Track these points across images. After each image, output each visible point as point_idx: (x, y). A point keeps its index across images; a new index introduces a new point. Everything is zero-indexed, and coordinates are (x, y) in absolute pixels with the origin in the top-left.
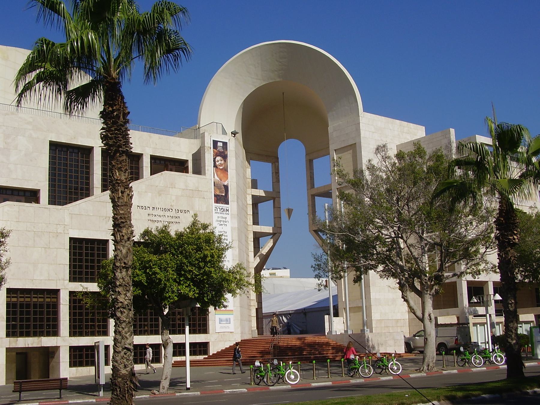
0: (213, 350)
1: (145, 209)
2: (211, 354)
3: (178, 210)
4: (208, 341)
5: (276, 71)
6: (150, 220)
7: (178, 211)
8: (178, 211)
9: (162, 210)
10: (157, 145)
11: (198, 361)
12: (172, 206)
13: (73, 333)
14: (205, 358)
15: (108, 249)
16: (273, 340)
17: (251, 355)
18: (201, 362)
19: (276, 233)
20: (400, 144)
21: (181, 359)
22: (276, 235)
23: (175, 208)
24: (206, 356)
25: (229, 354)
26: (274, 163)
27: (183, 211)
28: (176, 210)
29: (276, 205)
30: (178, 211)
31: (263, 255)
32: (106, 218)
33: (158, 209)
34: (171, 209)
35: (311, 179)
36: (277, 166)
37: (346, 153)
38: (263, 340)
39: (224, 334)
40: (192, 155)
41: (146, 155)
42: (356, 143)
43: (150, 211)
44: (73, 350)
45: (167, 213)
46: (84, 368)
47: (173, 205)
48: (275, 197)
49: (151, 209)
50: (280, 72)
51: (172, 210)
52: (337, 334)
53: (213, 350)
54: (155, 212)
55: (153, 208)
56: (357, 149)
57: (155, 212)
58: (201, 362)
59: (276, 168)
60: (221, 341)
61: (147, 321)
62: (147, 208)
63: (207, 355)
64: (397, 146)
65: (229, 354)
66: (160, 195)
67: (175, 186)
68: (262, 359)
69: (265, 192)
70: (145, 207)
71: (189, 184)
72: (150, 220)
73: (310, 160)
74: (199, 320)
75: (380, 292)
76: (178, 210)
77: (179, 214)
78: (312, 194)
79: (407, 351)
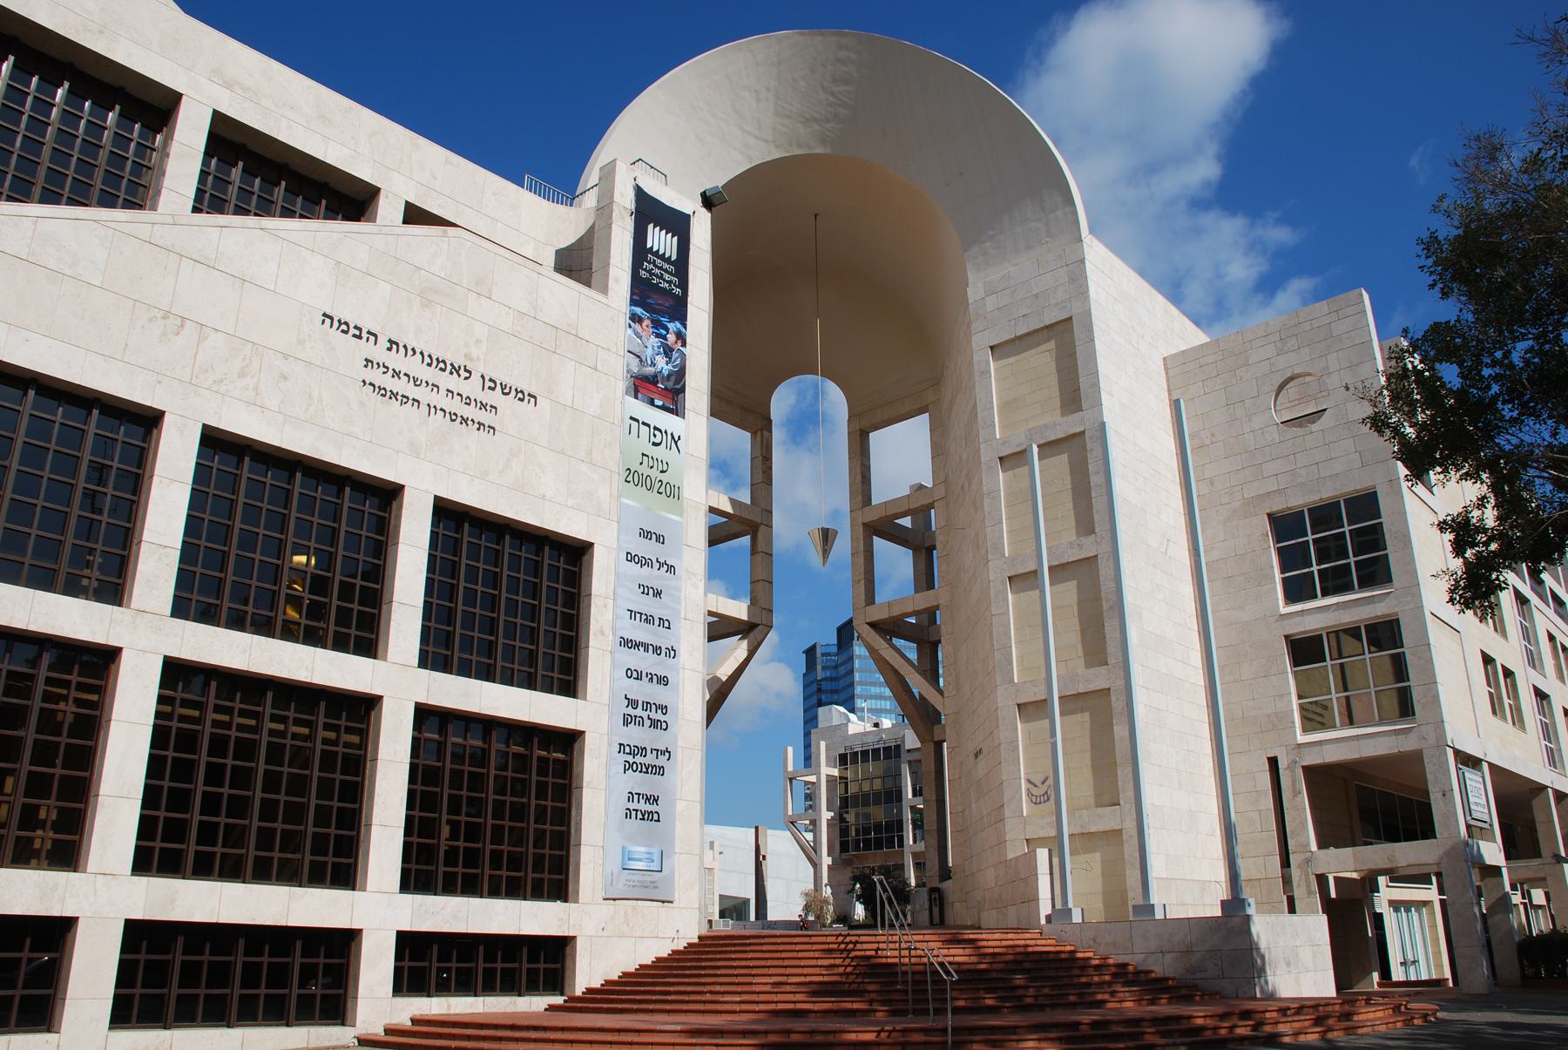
0: (588, 973)
1: (354, 336)
2: (579, 992)
4: (571, 934)
5: (815, 120)
6: (371, 384)
7: (492, 385)
8: (492, 385)
9: (427, 360)
10: (435, 178)
11: (513, 1027)
14: (551, 1008)
17: (780, 1006)
19: (758, 625)
21: (449, 1006)
23: (482, 371)
24: (558, 1000)
25: (669, 993)
27: (513, 392)
28: (483, 377)
29: (761, 546)
30: (492, 384)
31: (720, 683)
33: (410, 352)
34: (466, 370)
36: (768, 440)
37: (1032, 352)
38: (766, 940)
39: (634, 908)
40: (557, 251)
41: (390, 196)
42: (1070, 318)
43: (379, 353)
44: (411, 945)
45: (447, 381)
47: (475, 356)
48: (759, 521)
50: (828, 126)
51: (470, 372)
53: (588, 973)
54: (396, 360)
55: (390, 341)
57: (396, 360)
60: (623, 936)
62: (365, 335)
63: (562, 994)
64: (1165, 359)
65: (669, 993)
67: (490, 291)
68: (879, 1032)
69: (733, 502)
73: (861, 430)
74: (539, 841)
75: (1160, 785)
76: (491, 380)
77: (495, 397)
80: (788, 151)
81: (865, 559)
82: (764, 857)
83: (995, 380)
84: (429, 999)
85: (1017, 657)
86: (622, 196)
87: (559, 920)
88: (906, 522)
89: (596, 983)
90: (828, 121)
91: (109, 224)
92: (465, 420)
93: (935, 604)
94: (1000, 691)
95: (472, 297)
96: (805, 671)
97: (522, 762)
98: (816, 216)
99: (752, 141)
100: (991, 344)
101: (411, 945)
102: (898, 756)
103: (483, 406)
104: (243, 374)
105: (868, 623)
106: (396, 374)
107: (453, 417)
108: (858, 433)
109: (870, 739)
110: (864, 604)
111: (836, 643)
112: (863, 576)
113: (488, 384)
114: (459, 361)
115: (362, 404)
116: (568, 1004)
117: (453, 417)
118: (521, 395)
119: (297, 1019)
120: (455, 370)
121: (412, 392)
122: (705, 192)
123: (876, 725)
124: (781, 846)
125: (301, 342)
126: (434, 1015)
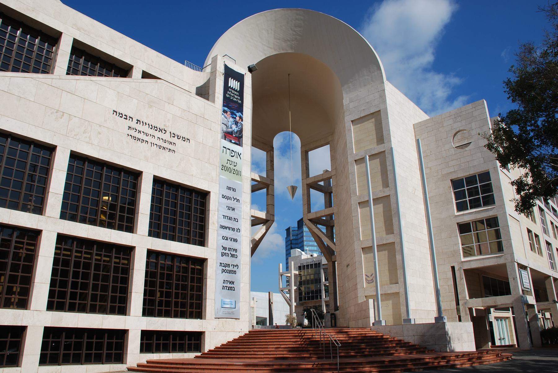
0: (209, 344)
1: (124, 118)
2: (206, 351)
3: (175, 135)
5: (289, 41)
6: (130, 135)
7: (174, 135)
8: (174, 135)
9: (151, 127)
11: (183, 364)
12: (166, 127)
13: (148, 312)
15: (52, 162)
16: (299, 332)
17: (278, 356)
18: (197, 367)
19: (269, 220)
20: (418, 123)
21: (160, 356)
22: (269, 222)
23: (170, 130)
24: (199, 354)
26: (269, 152)
27: (181, 138)
28: (170, 133)
29: (270, 192)
30: (174, 135)
31: (256, 241)
32: (56, 112)
33: (144, 124)
34: (164, 130)
35: (306, 169)
39: (226, 321)
40: (197, 88)
41: (137, 68)
42: (380, 110)
43: (133, 124)
44: (146, 335)
45: (158, 134)
46: (82, 366)
48: (270, 184)
49: (135, 121)
50: (293, 43)
51: (166, 131)
52: (416, 323)
53: (209, 344)
54: (139, 127)
56: (382, 116)
57: (139, 127)
58: (197, 367)
59: (271, 156)
61: (106, 301)
62: (128, 118)
63: (200, 352)
64: (414, 125)
66: (151, 107)
67: (173, 102)
69: (260, 177)
70: (125, 115)
71: (192, 106)
72: (131, 136)
76: (173, 134)
77: (175, 140)
78: (307, 183)
79: (121, 362)
80: (279, 52)
81: (307, 196)
82: (272, 303)
83: (353, 133)
84: (153, 354)
85: (362, 231)
86: (220, 68)
87: (199, 326)
88: (322, 183)
89: (212, 348)
90: (293, 41)
91: (37, 79)
92: (164, 148)
93: (332, 212)
94: (356, 243)
95: (167, 104)
96: (286, 237)
97: (186, 270)
98: (289, 75)
99: (266, 48)
100: (352, 120)
101: (146, 335)
102: (319, 267)
103: (171, 143)
104: (85, 132)
105: (308, 220)
106: (140, 132)
107: (160, 147)
108: (305, 152)
109: (310, 261)
110: (307, 213)
111: (297, 226)
112: (306, 203)
113: (172, 135)
114: (162, 127)
115: (127, 143)
116: (202, 356)
117: (160, 147)
118: (184, 139)
119: (106, 362)
120: (161, 130)
121: (145, 138)
122: (249, 66)
123: (312, 256)
124: (278, 298)
125: (105, 121)
126: (155, 360)
